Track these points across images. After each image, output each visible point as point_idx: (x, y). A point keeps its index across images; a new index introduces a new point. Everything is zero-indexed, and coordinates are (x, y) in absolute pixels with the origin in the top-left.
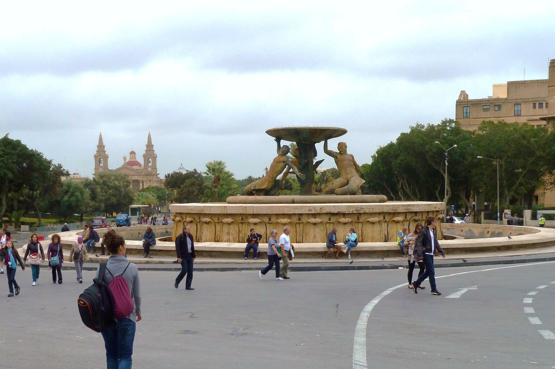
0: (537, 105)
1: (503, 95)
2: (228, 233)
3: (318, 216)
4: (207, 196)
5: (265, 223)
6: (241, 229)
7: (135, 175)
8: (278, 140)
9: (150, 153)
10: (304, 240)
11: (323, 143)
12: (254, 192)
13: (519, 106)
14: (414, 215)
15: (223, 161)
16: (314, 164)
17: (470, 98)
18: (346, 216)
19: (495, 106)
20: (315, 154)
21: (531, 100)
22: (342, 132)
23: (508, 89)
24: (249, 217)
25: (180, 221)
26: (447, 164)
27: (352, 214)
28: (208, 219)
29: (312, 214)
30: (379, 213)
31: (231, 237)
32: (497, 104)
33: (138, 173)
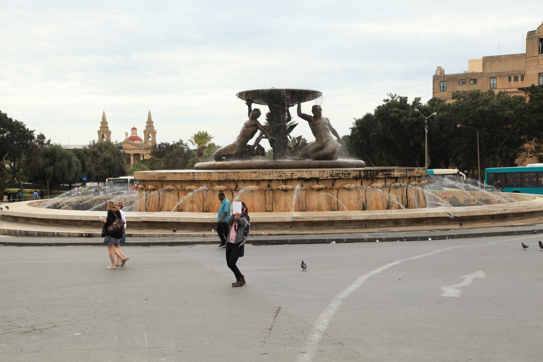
0: (512, 78)
1: (479, 69)
3: (289, 182)
5: (232, 191)
6: (205, 196)
7: (136, 149)
9: (150, 129)
10: (274, 209)
11: (296, 106)
13: (495, 80)
14: (394, 181)
15: (210, 134)
17: (445, 73)
18: (320, 182)
19: (471, 80)
20: (289, 119)
21: (506, 74)
23: (483, 63)
24: (214, 184)
25: (142, 189)
26: (427, 131)
27: (327, 179)
29: (283, 180)
31: (195, 206)
32: (473, 78)
33: (139, 147)
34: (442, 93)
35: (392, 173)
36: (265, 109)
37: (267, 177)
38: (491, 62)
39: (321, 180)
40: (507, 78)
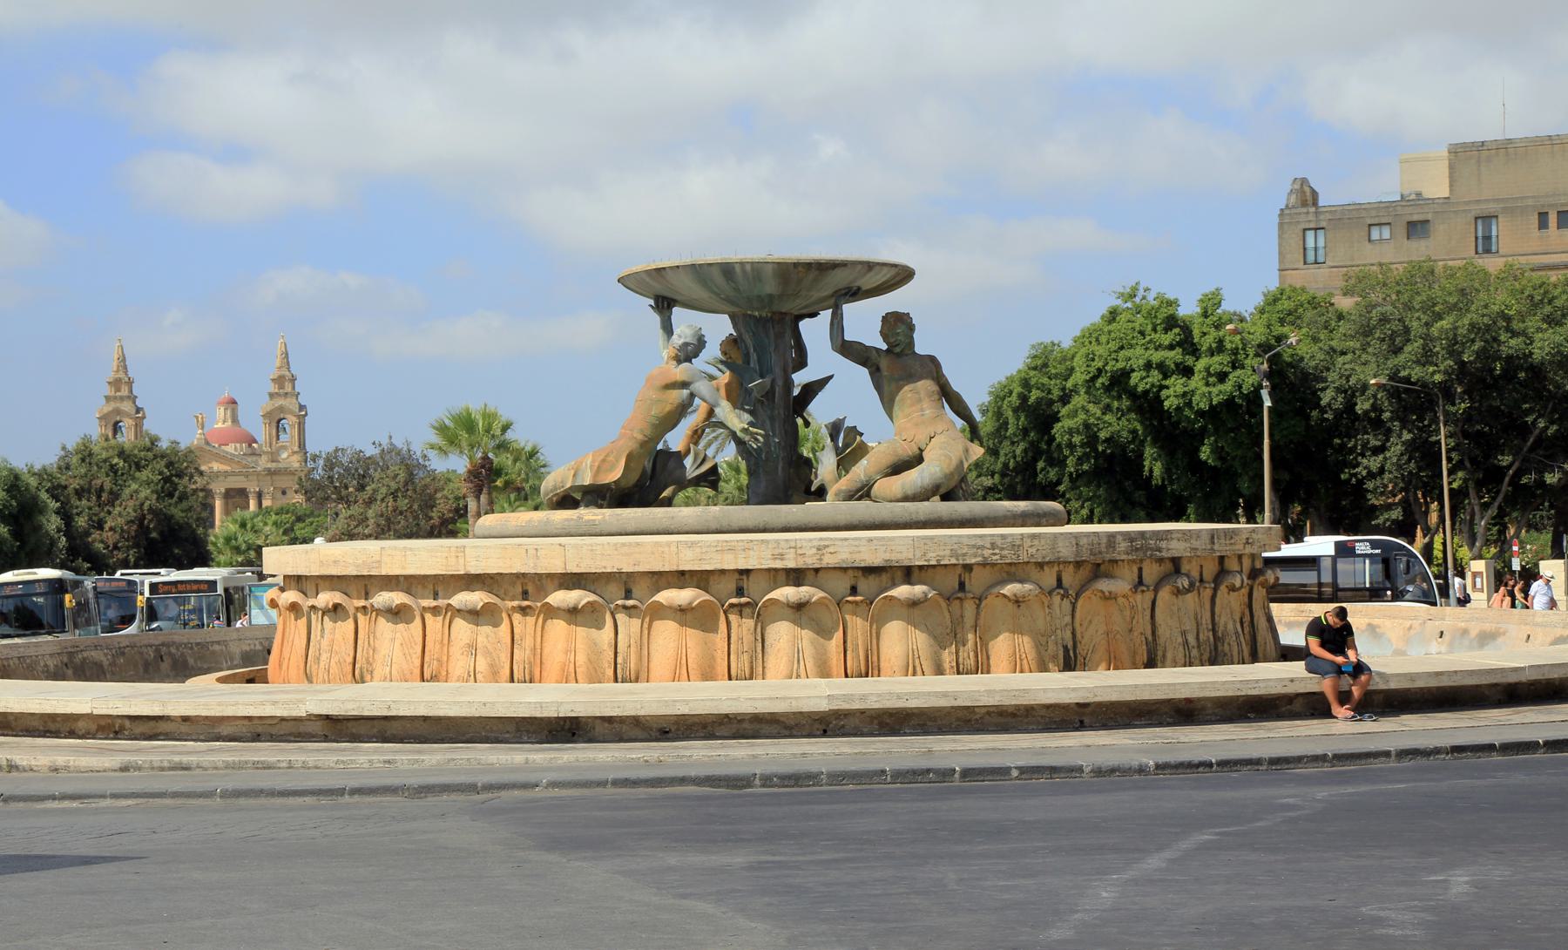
0: (1553, 219)
2: (472, 648)
4: (914, 727)
8: (664, 305)
11: (826, 315)
12: (578, 496)
16: (796, 392)
22: (902, 275)
23: (1451, 167)
28: (396, 598)
29: (788, 571)
30: (1041, 565)
31: (482, 664)
34: (1313, 271)
35: (1163, 544)
36: (718, 327)
37: (729, 563)
38: (1479, 161)
39: (921, 567)
40: (1535, 219)
